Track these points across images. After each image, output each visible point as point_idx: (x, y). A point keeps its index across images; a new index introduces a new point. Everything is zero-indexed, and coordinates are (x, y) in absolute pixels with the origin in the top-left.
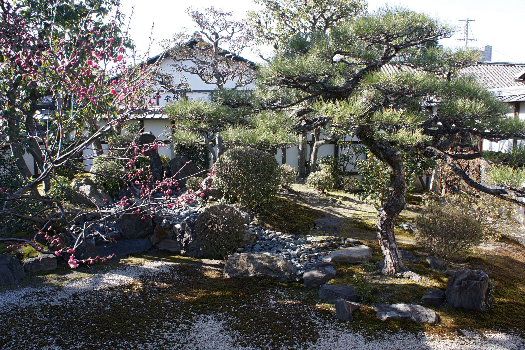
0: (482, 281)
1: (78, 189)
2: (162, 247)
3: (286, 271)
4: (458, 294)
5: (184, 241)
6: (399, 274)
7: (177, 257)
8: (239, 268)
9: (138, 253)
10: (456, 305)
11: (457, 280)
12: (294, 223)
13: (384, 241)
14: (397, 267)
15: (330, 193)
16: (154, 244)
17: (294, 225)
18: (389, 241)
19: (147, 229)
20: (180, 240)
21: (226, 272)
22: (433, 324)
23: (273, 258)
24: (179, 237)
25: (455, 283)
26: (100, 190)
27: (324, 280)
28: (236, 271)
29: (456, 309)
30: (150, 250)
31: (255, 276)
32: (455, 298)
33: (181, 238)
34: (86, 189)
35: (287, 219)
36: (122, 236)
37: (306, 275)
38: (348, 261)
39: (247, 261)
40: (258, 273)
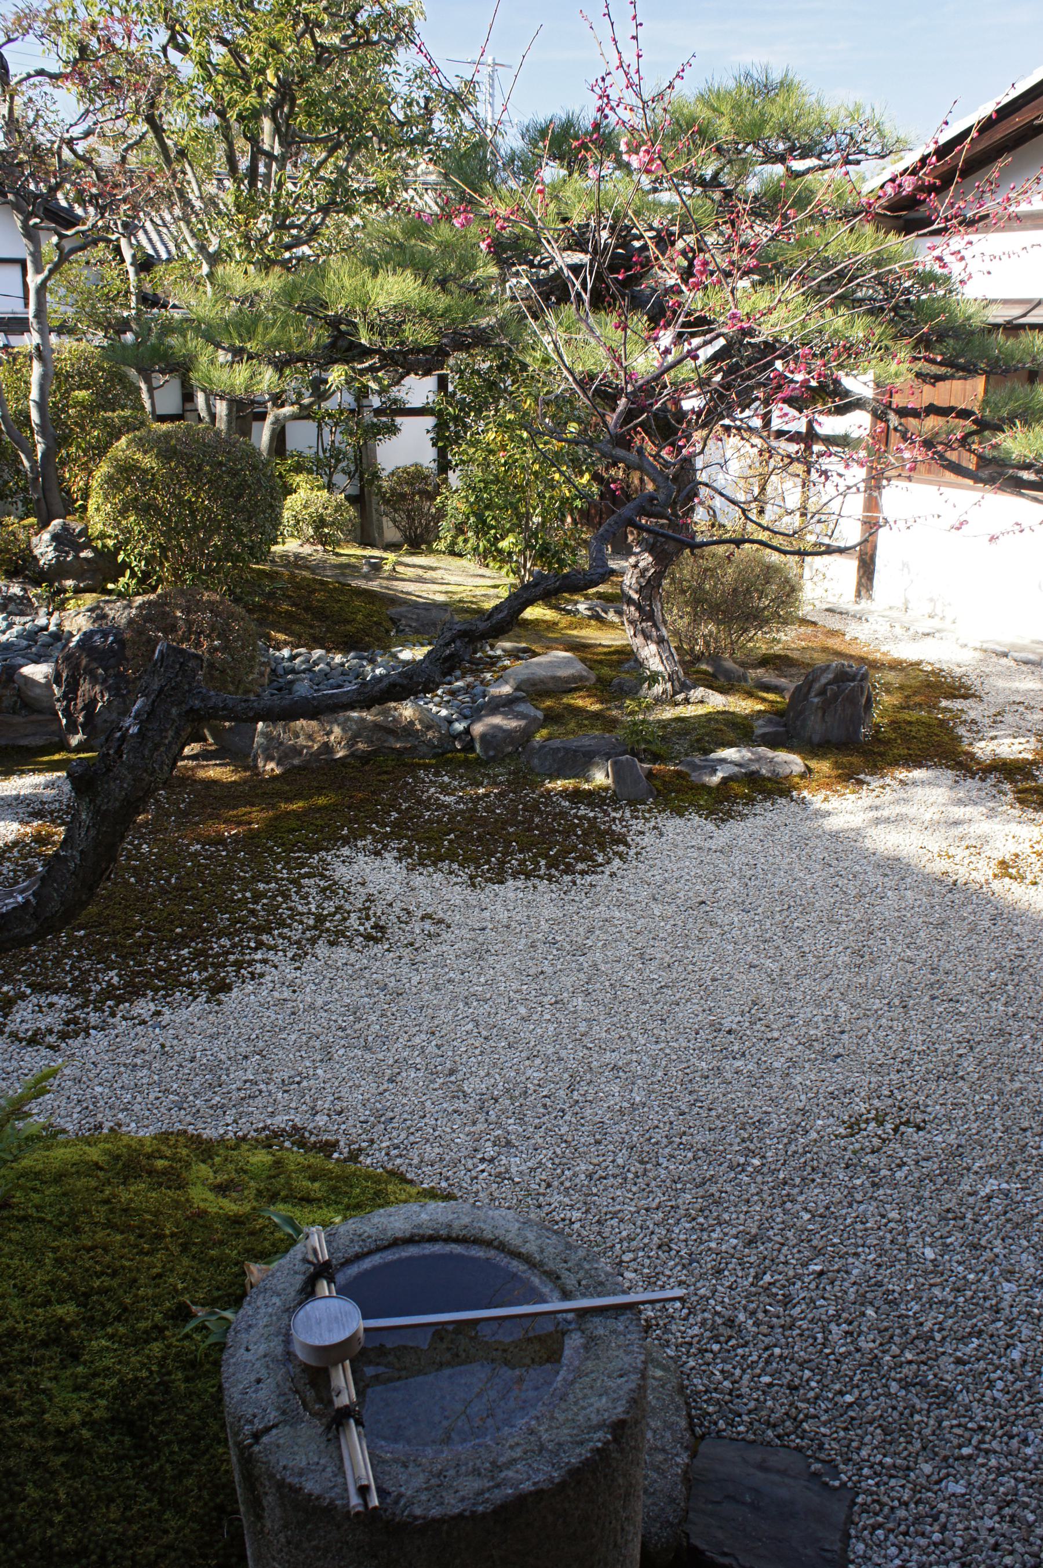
0: (861, 680)
3: (429, 727)
4: (820, 714)
5: (80, 706)
6: (680, 697)
7: (57, 757)
8: (302, 741)
10: (816, 739)
11: (817, 686)
12: (348, 622)
13: (644, 624)
14: (676, 683)
15: (342, 551)
17: (348, 627)
18: (655, 625)
21: (269, 758)
22: (802, 776)
25: (813, 694)
27: (527, 734)
28: (296, 751)
29: (820, 745)
31: (352, 755)
32: (815, 726)
33: (69, 701)
35: (320, 614)
37: (478, 729)
38: (551, 686)
40: (360, 746)
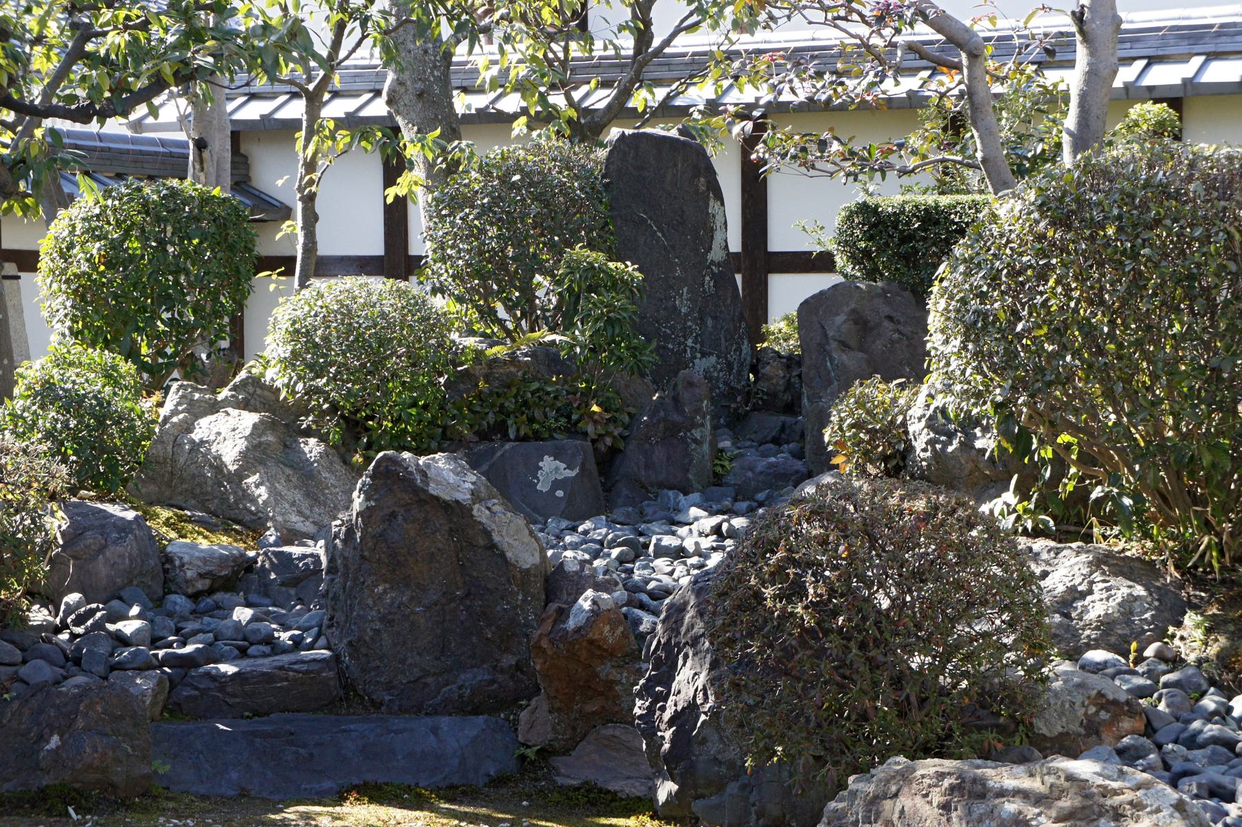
1: (188, 427)
2: (571, 772)
5: (667, 716)
9: (409, 789)
16: (531, 753)
19: (509, 660)
20: (651, 710)
23: (1106, 792)
24: (647, 691)
26: (312, 448)
30: (499, 781)
34: (227, 433)
36: (347, 685)
39: (946, 807)
